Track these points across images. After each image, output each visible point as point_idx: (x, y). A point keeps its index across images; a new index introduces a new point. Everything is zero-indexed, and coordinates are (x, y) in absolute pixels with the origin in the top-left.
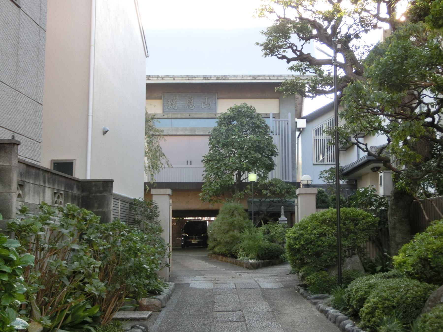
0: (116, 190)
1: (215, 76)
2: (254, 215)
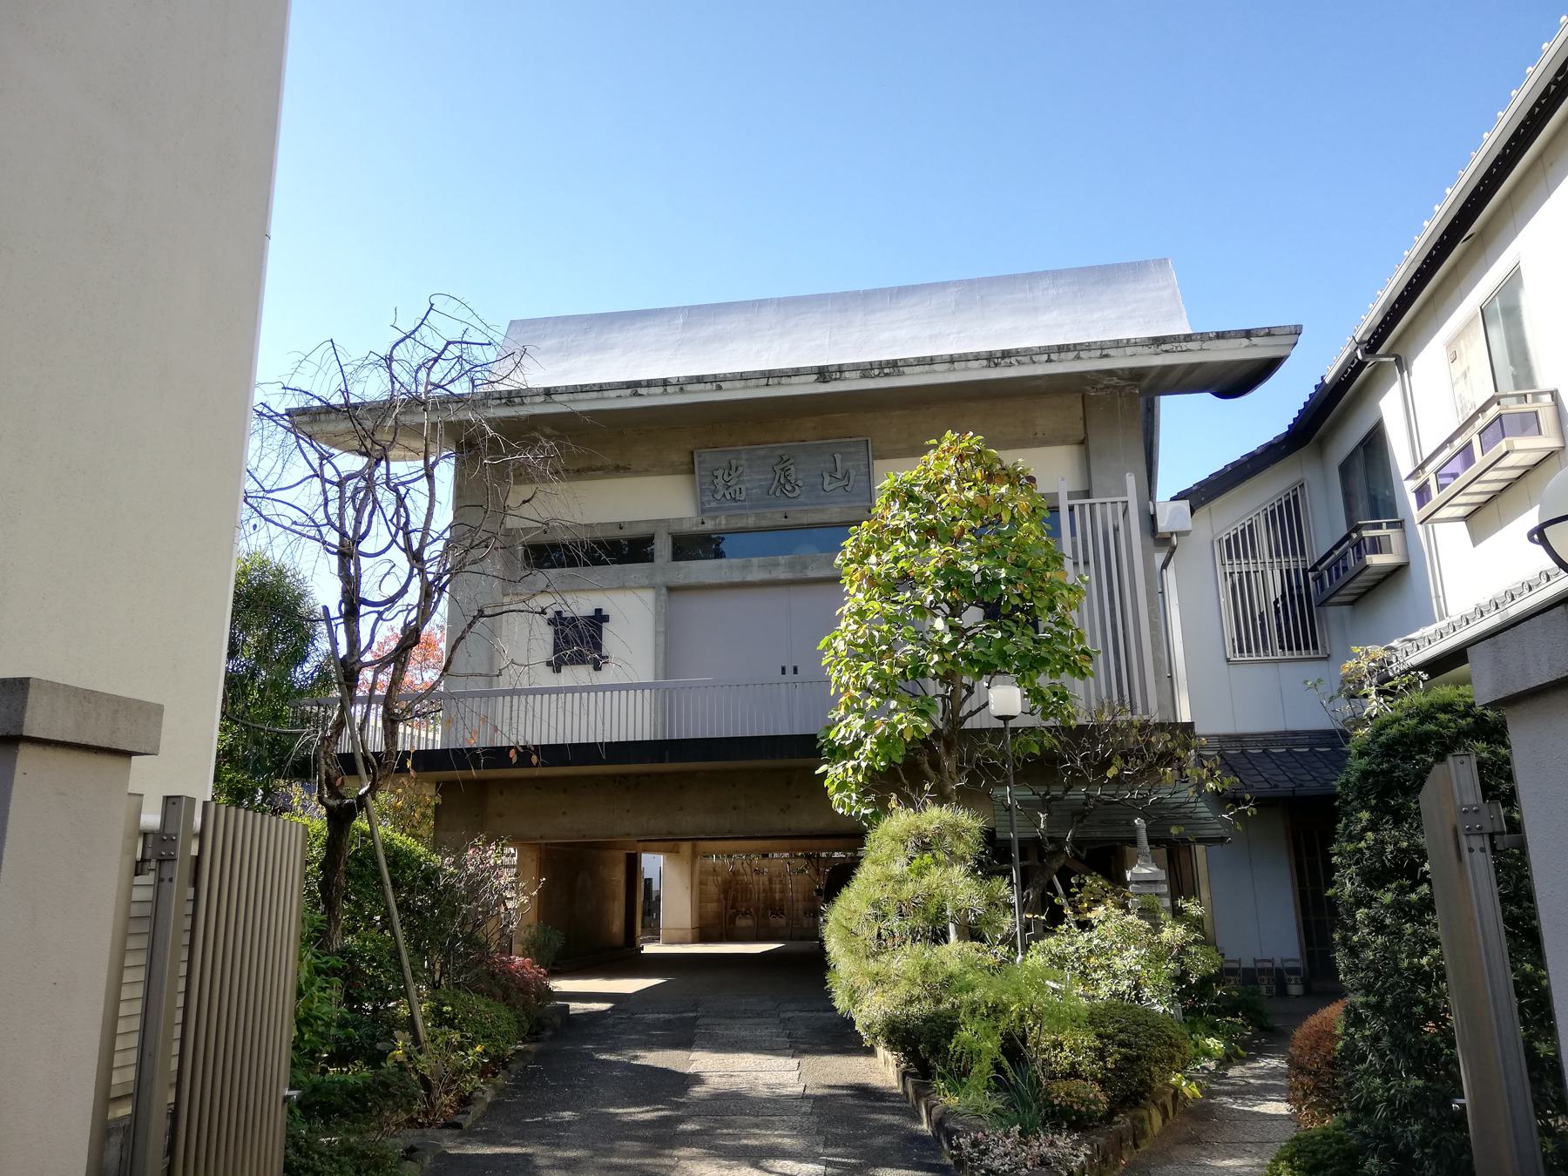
0: (1198, 730)
1: (856, 367)
2: (1023, 857)
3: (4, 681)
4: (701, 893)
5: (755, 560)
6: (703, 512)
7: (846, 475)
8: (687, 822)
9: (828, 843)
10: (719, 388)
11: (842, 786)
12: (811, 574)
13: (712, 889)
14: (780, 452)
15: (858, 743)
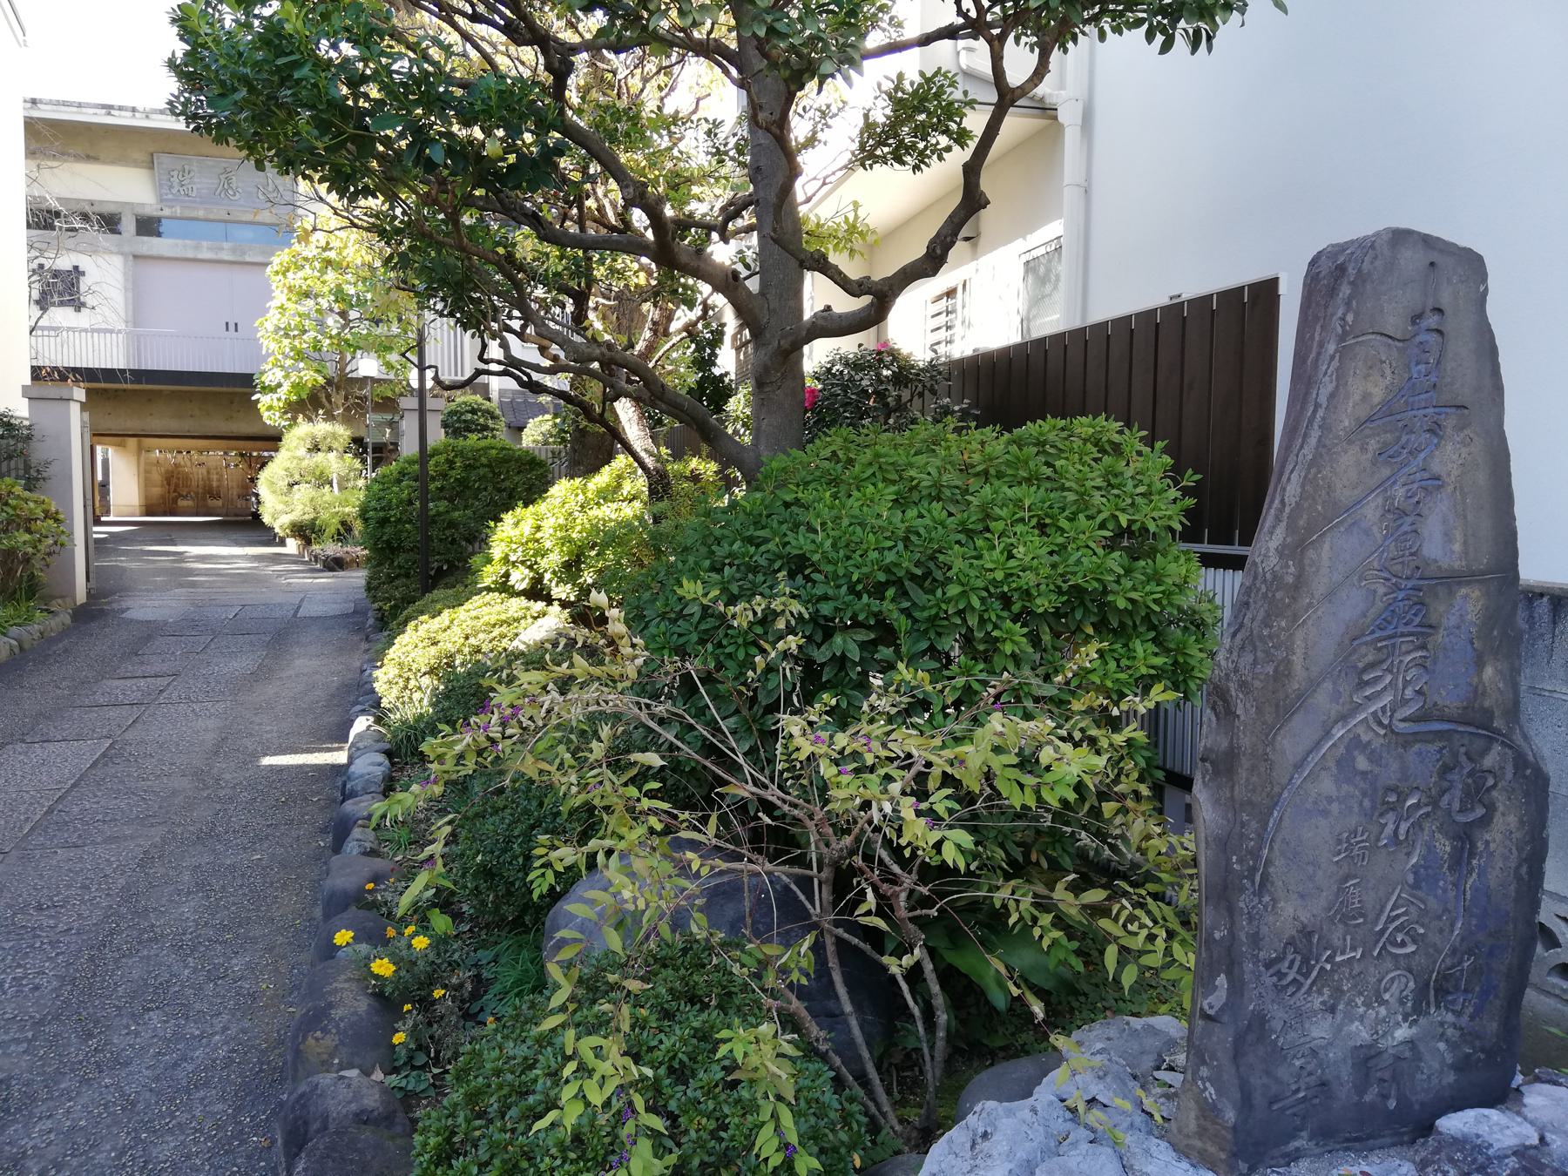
4: (146, 479)
5: (205, 243)
8: (156, 423)
9: (259, 444)
11: (270, 408)
12: (248, 259)
13: (157, 477)
15: (279, 385)
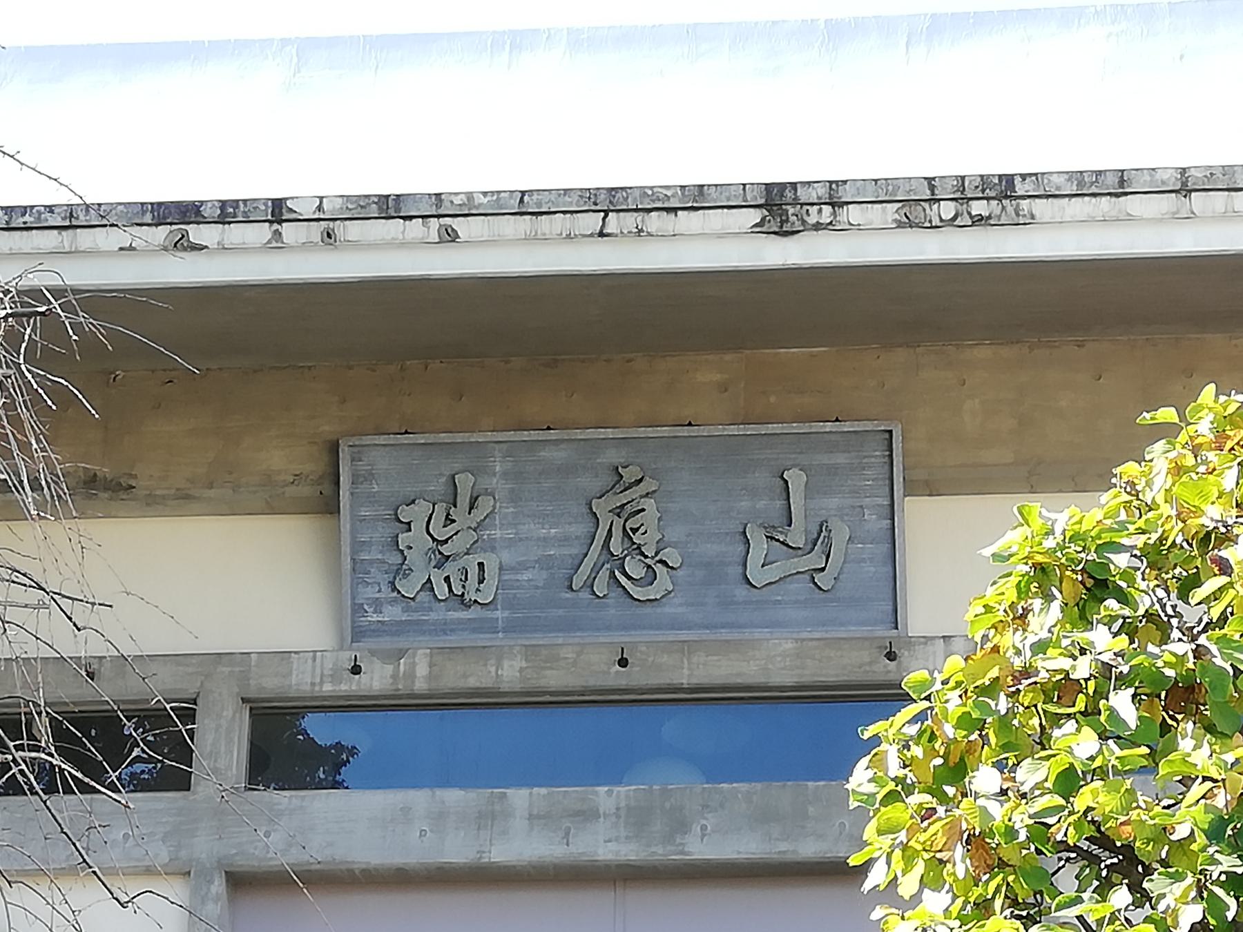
1: (883, 192)
3: (193, 366)
5: (520, 798)
6: (358, 634)
7: (820, 537)
10: (450, 236)
14: (613, 456)
